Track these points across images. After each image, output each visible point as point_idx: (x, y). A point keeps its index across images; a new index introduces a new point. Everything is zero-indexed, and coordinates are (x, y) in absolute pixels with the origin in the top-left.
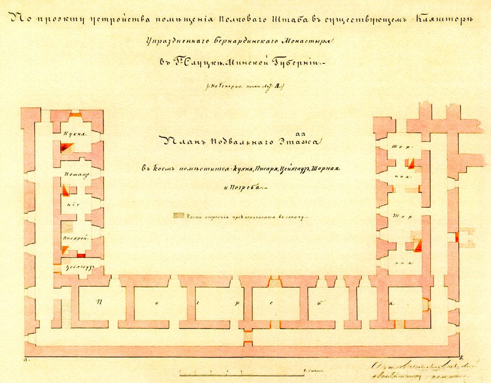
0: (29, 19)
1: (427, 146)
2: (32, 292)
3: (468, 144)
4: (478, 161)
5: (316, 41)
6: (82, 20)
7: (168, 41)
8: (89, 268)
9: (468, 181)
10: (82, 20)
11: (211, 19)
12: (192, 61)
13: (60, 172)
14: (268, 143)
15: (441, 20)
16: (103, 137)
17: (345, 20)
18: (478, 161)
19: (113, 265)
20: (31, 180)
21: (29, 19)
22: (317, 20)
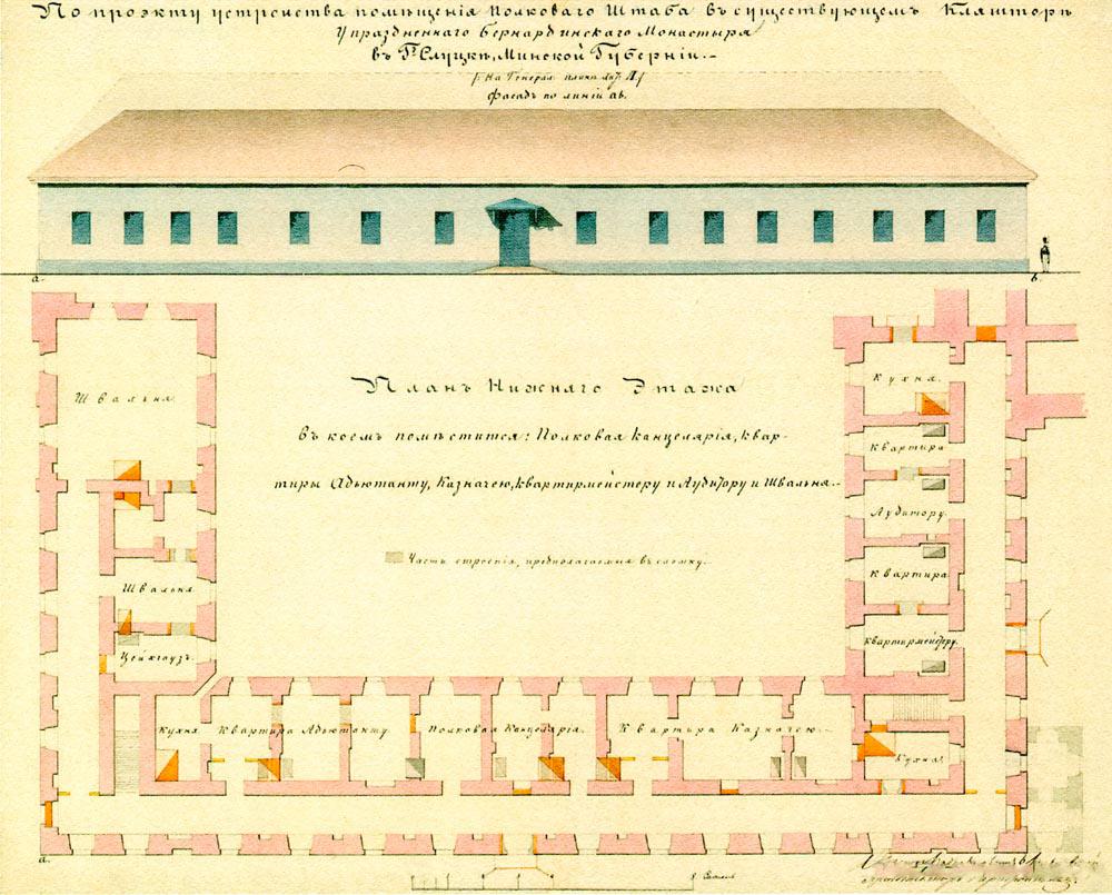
0: (76, 13)
1: (958, 373)
2: (51, 664)
3: (1050, 371)
4: (1070, 407)
5: (714, 34)
6: (196, 14)
7: (383, 34)
8: (176, 661)
9: (1051, 445)
10: (196, 14)
11: (472, 12)
12: (432, 54)
13: (113, 586)
14: (589, 389)
15: (1000, 11)
16: (217, 521)
17: (777, 11)
18: (1070, 407)
19: (238, 655)
20: (52, 745)
21: (76, 13)
22: (718, 11)
